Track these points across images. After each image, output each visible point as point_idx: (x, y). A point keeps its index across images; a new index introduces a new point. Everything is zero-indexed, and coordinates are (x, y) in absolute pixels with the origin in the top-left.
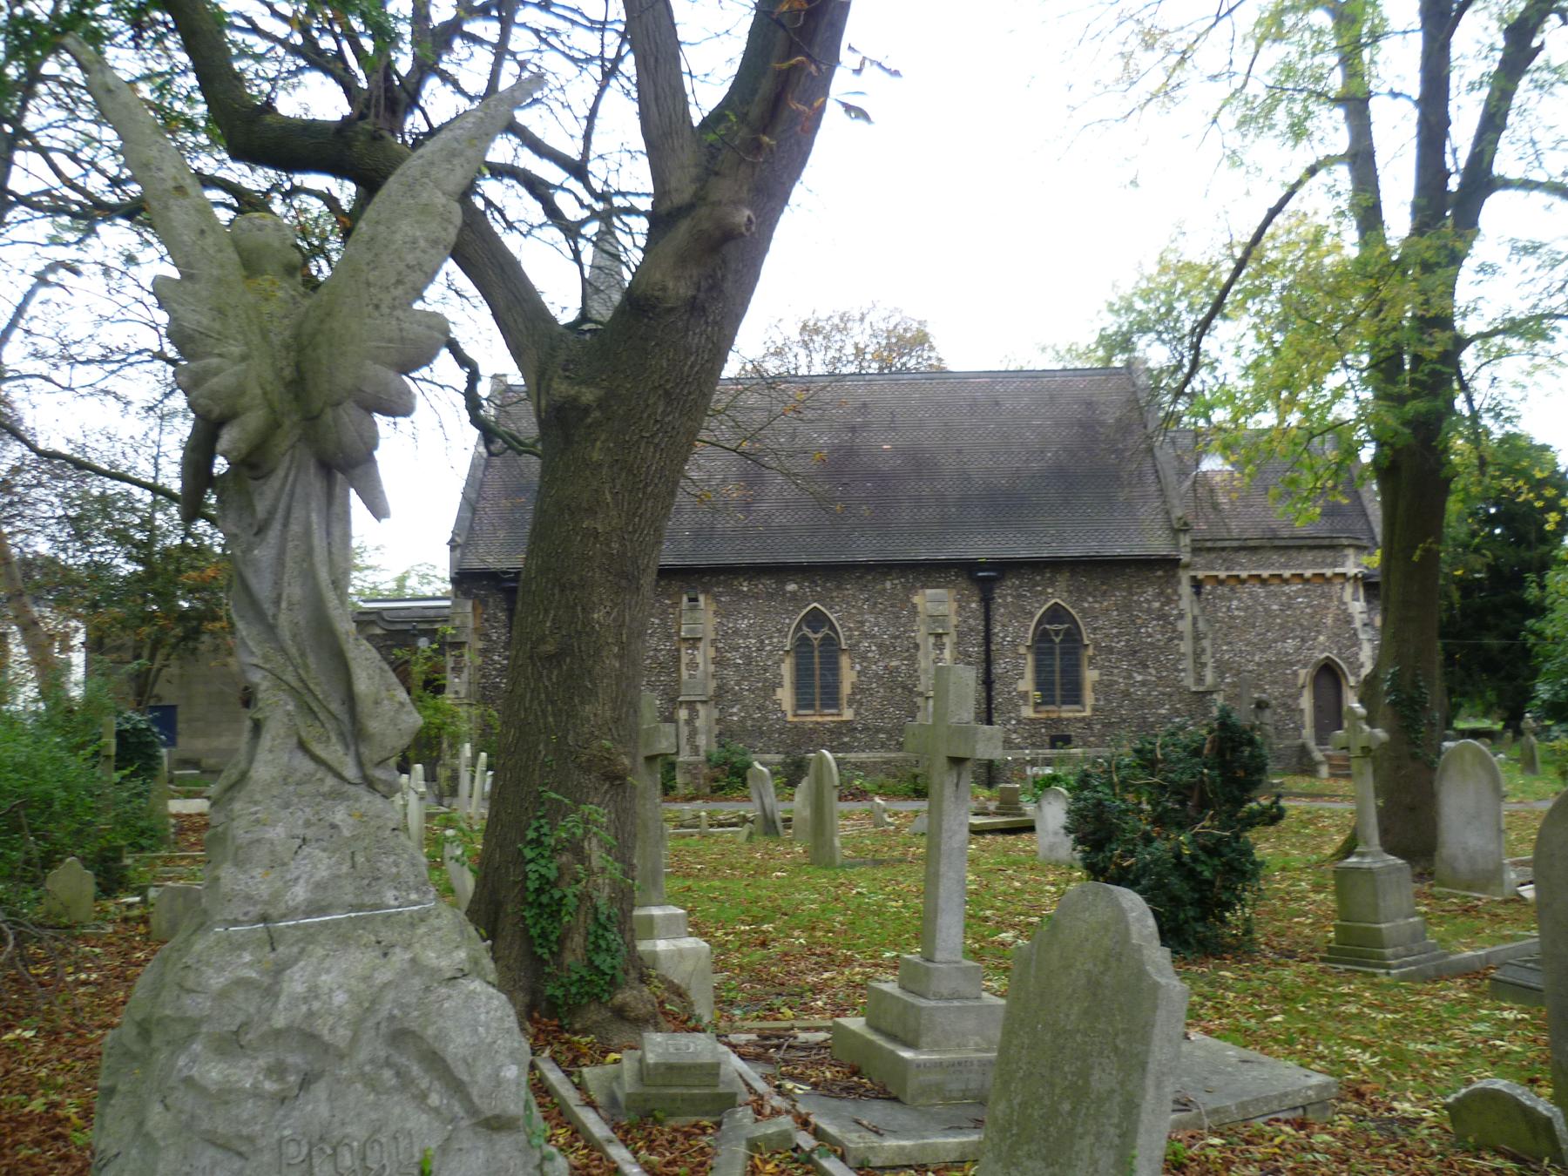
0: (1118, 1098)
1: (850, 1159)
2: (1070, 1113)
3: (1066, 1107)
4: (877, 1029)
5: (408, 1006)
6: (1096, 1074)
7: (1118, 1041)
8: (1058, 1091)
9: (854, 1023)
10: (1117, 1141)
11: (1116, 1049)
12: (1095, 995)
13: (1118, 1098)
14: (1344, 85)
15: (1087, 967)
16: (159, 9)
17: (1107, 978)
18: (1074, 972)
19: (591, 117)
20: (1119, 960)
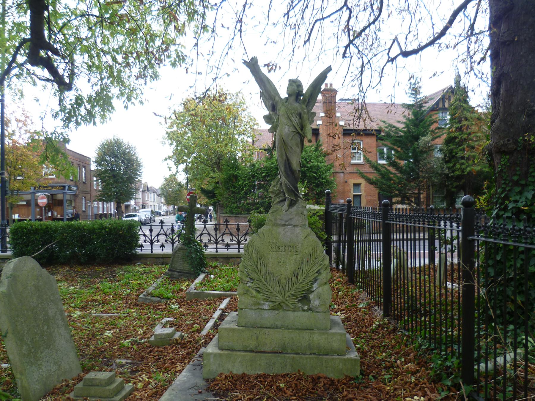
0: (58, 313)
1: (205, 370)
2: (48, 329)
3: (46, 327)
4: (222, 349)
5: (197, 12)
6: (50, 311)
7: (51, 298)
8: (41, 326)
9: (134, 376)
10: (63, 323)
11: (51, 301)
12: (39, 290)
13: (58, 313)
14: (208, 255)
15: (33, 283)
16: (474, 356)
17: (40, 283)
18: (29, 288)
19: (383, 69)
20: (41, 276)
